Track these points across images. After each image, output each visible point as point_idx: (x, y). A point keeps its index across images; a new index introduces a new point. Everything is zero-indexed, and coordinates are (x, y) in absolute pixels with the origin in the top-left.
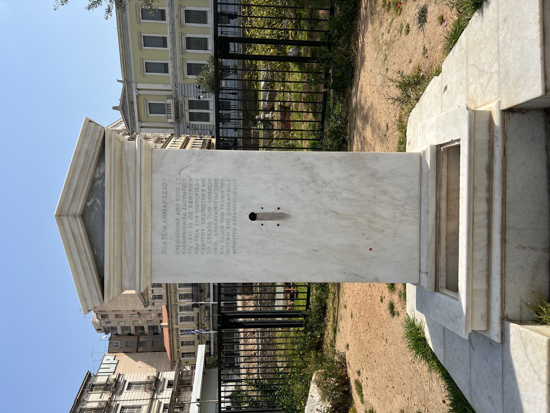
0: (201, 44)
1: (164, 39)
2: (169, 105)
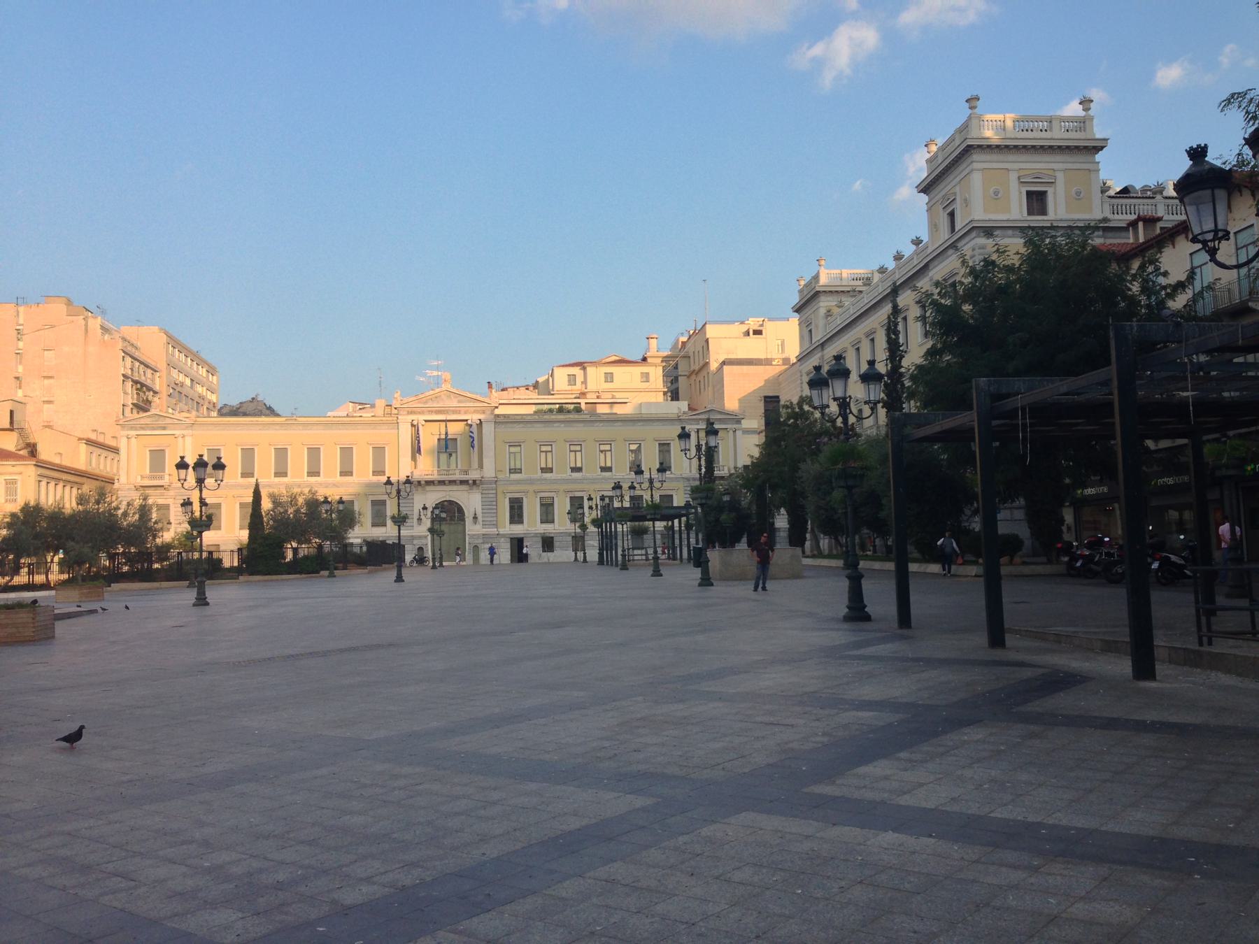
0: (547, 517)
1: (7, 482)
2: (161, 478)
